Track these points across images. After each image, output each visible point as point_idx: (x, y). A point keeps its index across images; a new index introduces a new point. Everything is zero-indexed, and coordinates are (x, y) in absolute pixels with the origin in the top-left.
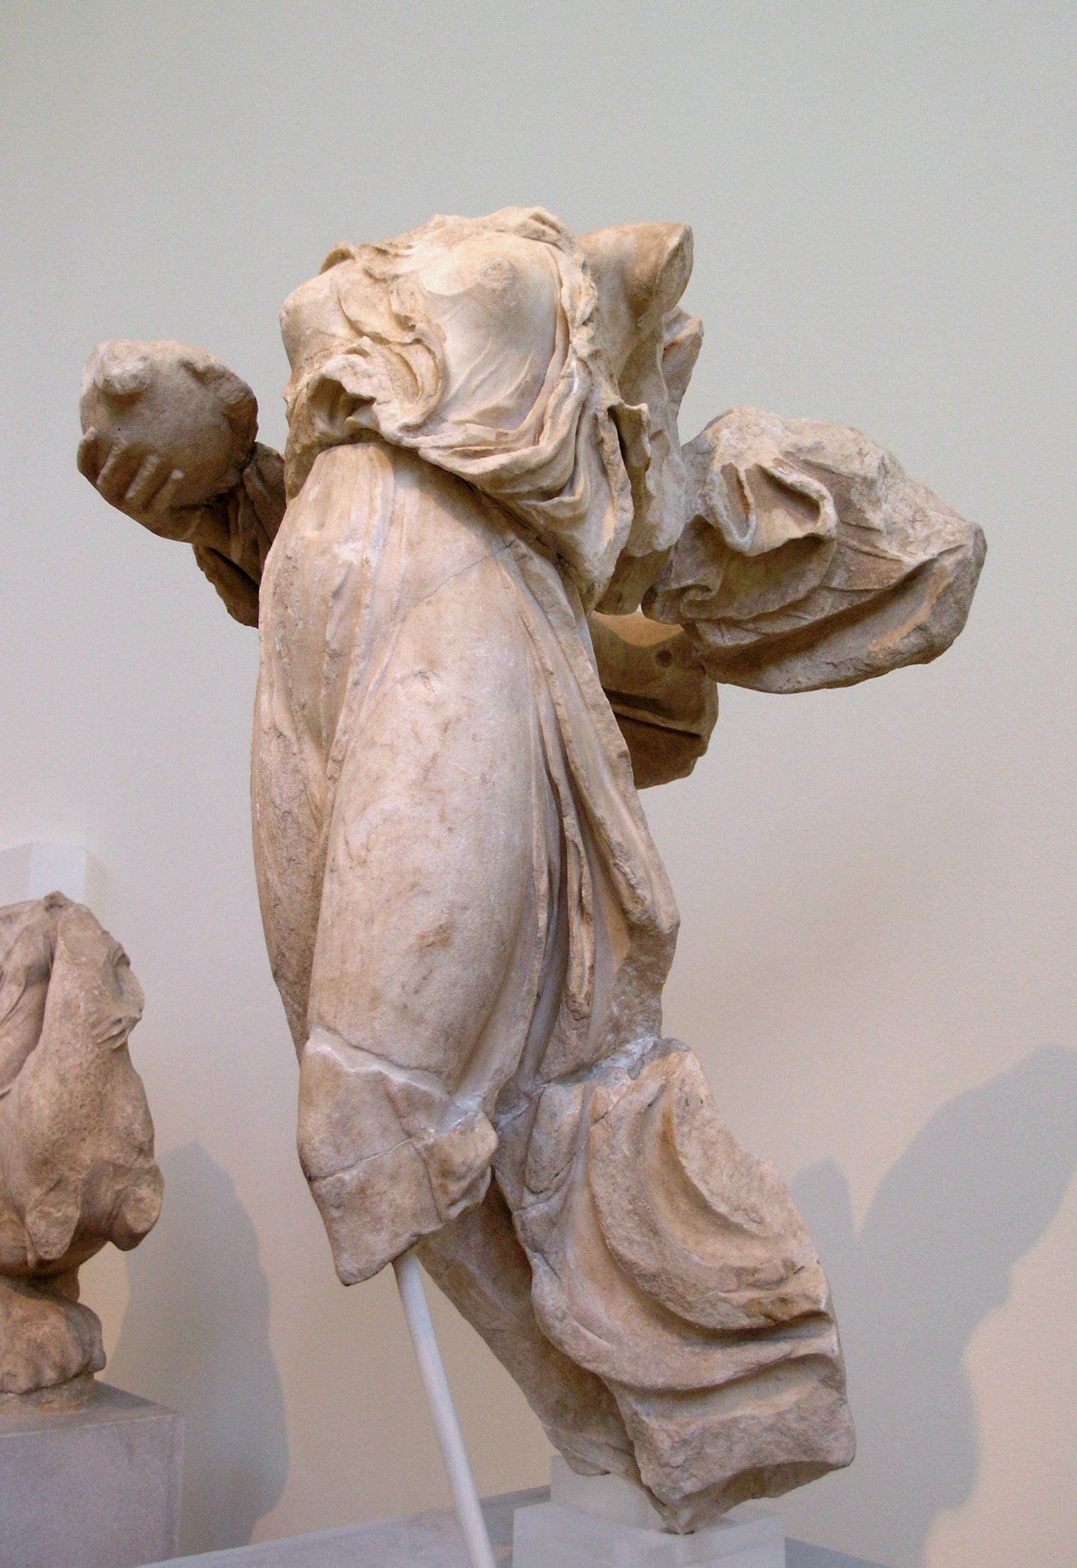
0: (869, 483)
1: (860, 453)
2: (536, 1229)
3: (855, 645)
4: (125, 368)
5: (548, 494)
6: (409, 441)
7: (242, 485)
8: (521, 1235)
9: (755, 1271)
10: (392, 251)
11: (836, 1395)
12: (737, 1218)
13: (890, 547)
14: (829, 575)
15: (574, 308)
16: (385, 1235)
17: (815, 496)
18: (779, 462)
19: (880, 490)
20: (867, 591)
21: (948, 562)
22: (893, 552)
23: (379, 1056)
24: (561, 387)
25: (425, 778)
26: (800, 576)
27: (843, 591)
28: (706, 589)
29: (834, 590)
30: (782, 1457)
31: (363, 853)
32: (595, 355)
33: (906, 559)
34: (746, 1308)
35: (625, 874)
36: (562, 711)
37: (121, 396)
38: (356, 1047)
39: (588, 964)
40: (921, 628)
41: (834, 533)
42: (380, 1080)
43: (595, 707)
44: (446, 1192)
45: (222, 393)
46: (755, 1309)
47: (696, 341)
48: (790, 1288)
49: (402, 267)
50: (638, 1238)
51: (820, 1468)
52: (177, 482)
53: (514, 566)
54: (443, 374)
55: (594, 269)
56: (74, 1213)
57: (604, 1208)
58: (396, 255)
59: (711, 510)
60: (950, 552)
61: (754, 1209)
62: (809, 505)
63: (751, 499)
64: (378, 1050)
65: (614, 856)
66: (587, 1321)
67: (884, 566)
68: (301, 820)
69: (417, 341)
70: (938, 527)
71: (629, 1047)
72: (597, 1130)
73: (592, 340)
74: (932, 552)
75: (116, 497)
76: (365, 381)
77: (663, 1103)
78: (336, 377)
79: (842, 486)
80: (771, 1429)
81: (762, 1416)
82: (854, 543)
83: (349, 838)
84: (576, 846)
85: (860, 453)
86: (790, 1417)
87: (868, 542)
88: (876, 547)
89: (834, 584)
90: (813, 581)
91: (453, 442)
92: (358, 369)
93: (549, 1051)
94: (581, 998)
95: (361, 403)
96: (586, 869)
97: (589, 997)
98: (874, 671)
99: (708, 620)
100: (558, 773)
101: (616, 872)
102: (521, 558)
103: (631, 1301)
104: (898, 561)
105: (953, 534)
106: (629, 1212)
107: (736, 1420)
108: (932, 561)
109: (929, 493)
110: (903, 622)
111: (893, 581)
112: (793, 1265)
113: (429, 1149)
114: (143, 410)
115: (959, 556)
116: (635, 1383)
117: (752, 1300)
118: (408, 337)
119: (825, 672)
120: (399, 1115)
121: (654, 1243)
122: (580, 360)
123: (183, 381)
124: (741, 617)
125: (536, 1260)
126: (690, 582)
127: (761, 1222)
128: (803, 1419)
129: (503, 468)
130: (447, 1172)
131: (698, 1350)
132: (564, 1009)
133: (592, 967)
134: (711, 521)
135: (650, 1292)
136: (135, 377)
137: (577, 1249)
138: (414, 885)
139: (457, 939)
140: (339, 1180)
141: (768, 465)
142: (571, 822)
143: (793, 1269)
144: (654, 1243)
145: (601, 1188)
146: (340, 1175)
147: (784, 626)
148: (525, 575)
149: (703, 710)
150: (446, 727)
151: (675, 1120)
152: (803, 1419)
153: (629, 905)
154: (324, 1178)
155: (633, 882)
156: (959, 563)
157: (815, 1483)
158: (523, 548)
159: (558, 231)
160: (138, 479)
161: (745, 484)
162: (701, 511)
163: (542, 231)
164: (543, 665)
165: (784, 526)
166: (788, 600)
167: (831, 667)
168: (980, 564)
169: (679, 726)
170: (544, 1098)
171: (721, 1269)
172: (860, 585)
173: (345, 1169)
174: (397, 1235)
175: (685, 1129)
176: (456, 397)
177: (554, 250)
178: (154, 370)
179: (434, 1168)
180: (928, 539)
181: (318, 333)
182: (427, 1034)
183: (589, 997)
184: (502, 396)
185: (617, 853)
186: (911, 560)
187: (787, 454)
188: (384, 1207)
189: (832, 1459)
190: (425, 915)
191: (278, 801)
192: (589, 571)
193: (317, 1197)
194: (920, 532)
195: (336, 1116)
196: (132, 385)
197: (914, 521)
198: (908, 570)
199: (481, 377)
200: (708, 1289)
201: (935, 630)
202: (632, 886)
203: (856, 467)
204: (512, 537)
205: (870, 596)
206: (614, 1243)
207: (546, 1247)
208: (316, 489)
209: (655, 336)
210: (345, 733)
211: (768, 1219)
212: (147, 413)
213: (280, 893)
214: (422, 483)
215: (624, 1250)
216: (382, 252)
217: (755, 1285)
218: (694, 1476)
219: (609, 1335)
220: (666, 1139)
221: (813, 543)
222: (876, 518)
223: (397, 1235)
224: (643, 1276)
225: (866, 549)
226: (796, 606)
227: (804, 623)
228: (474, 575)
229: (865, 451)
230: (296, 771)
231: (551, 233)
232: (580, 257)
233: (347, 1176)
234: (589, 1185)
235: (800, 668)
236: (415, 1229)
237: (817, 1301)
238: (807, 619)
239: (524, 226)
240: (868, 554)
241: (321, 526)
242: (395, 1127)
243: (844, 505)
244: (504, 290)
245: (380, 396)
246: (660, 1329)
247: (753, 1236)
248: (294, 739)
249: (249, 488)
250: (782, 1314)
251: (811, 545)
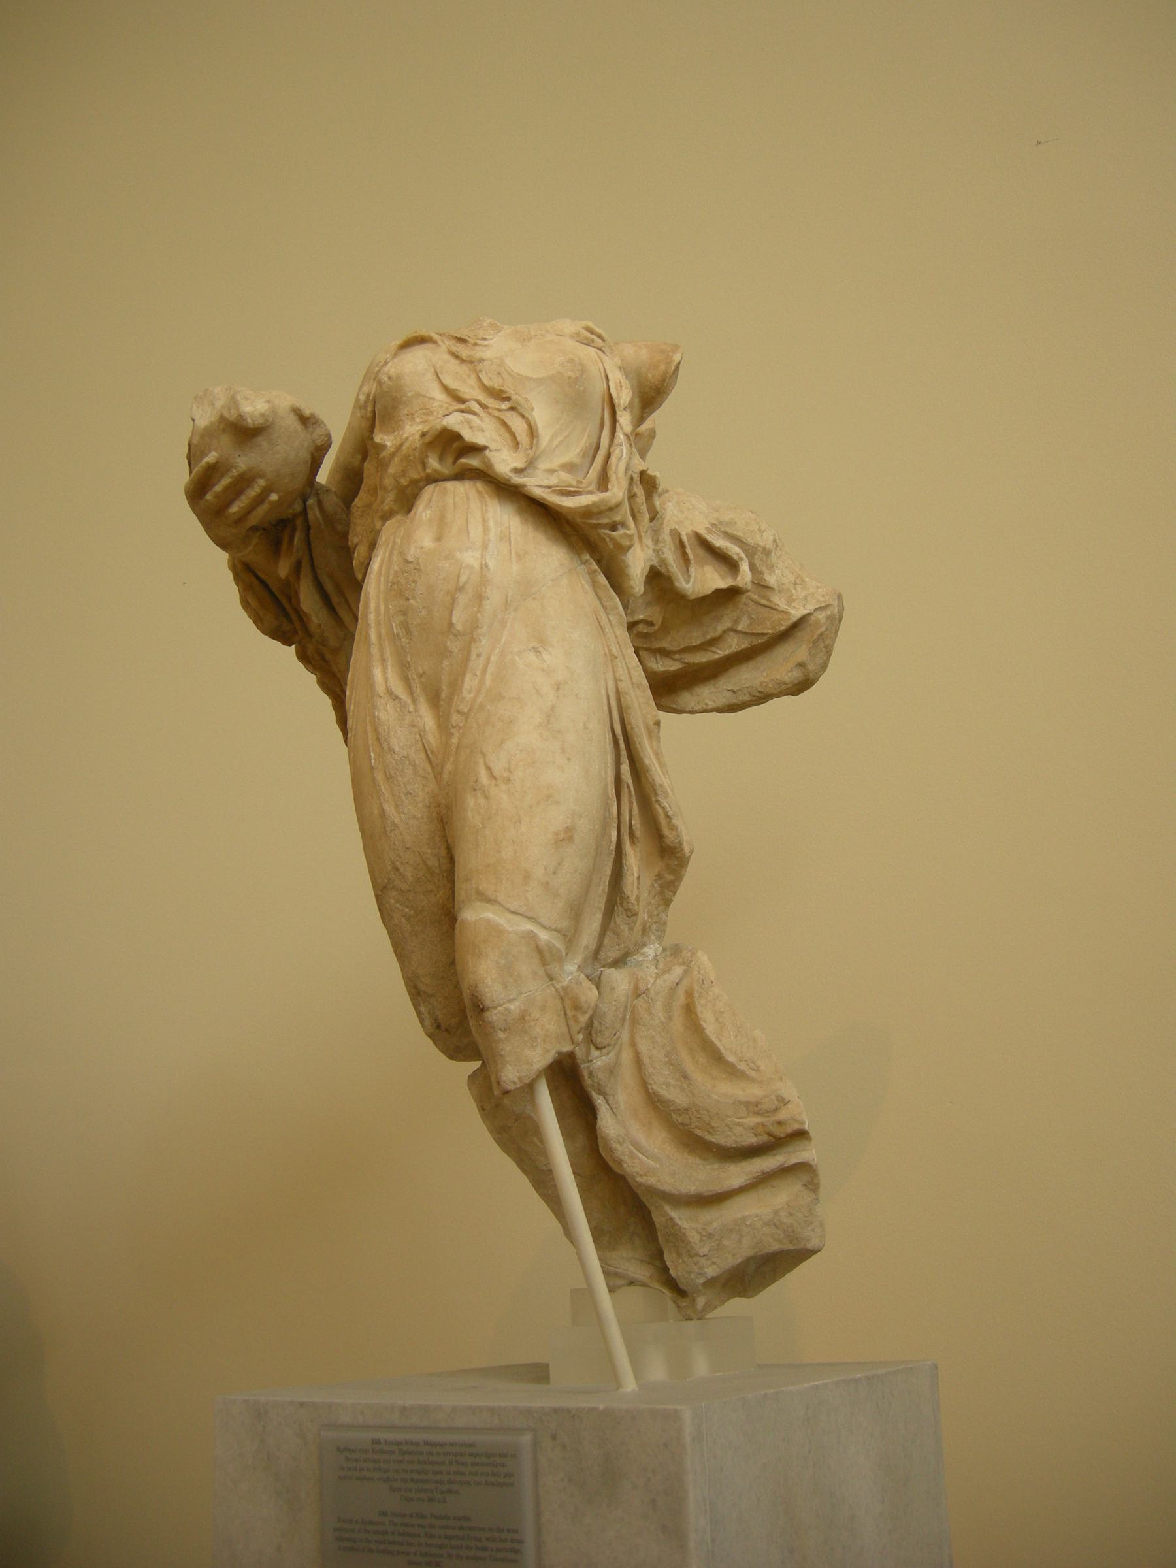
0: (767, 552)
2: (601, 1076)
3: (748, 677)
4: (254, 407)
6: (516, 480)
7: (305, 511)
9: (757, 1104)
10: (472, 341)
11: (813, 1195)
12: (742, 1066)
13: (779, 601)
14: (736, 621)
15: (619, 397)
16: (539, 1050)
17: (736, 558)
19: (773, 559)
20: (763, 634)
22: (783, 605)
23: (530, 918)
25: (549, 722)
26: (718, 619)
27: (746, 633)
28: (651, 624)
29: (741, 632)
30: (776, 1247)
31: (506, 774)
33: (793, 612)
34: (754, 1130)
35: (664, 808)
36: (621, 685)
37: (248, 429)
38: (513, 912)
39: (636, 875)
40: (801, 665)
41: (749, 586)
42: (531, 937)
43: (639, 686)
44: (577, 1021)
45: (315, 436)
46: (760, 1129)
48: (782, 1115)
49: (480, 353)
50: (672, 1082)
51: (804, 1254)
52: (271, 503)
53: (588, 578)
54: (532, 432)
57: (646, 1061)
58: (476, 344)
59: (663, 562)
60: (821, 609)
62: (731, 565)
63: (691, 556)
64: (530, 914)
65: (656, 795)
66: (636, 1145)
67: (776, 616)
68: (417, 762)
69: (512, 409)
70: (812, 590)
71: (646, 950)
72: (640, 1003)
76: (480, 433)
77: (685, 984)
78: (456, 428)
79: (751, 551)
81: (758, 1216)
83: (491, 765)
84: (628, 787)
85: (760, 530)
86: (783, 1213)
87: (765, 597)
88: (770, 601)
89: (739, 628)
90: (727, 623)
91: (551, 484)
92: (473, 424)
93: (606, 941)
94: (633, 899)
95: (475, 449)
96: (635, 805)
97: (638, 898)
98: (762, 698)
99: (647, 649)
100: (618, 731)
101: (657, 806)
102: (592, 573)
104: (787, 613)
105: (823, 596)
106: (666, 1063)
107: (744, 1219)
108: (809, 614)
111: (783, 628)
112: (783, 1099)
113: (565, 989)
114: (262, 441)
116: (674, 1191)
117: (758, 1124)
118: (505, 405)
119: (723, 699)
120: (544, 963)
121: (685, 1086)
122: (626, 435)
123: (292, 422)
124: (672, 649)
125: (599, 1101)
126: (641, 617)
127: (757, 1070)
128: (791, 1214)
129: (594, 504)
130: (577, 1007)
131: (716, 1166)
132: (619, 909)
133: (638, 878)
134: (663, 570)
135: (683, 1124)
136: (263, 415)
138: (549, 797)
140: (506, 1009)
141: (702, 531)
142: (625, 768)
143: (784, 1102)
144: (685, 1086)
145: (643, 1046)
146: (507, 1005)
148: (594, 584)
150: (558, 687)
151: (696, 994)
152: (791, 1214)
153: (666, 831)
154: (495, 1008)
155: (670, 814)
156: (828, 618)
157: (795, 1271)
158: (595, 566)
159: (603, 340)
160: (243, 498)
161: (687, 544)
162: (655, 563)
163: (592, 338)
164: (610, 651)
166: (708, 637)
167: (731, 694)
170: (603, 977)
171: (733, 1103)
173: (510, 1001)
174: (548, 1051)
175: (703, 1001)
177: (600, 353)
178: (274, 412)
179: (568, 1003)
180: (805, 598)
181: (418, 395)
182: (561, 905)
183: (638, 898)
185: (659, 792)
186: (796, 613)
187: (713, 525)
188: (538, 1030)
189: (810, 1246)
190: (557, 818)
191: (397, 749)
192: (632, 588)
194: (800, 593)
195: (503, 962)
196: (260, 421)
197: (795, 584)
198: (794, 619)
199: (560, 439)
200: (727, 1116)
202: (669, 817)
205: (765, 638)
206: (655, 1087)
207: (607, 1090)
208: (428, 512)
210: (470, 692)
211: (763, 1068)
212: (265, 444)
213: (397, 821)
214: (521, 511)
215: (664, 1092)
216: (461, 340)
217: (757, 1113)
218: (714, 1263)
220: (689, 1010)
222: (771, 580)
223: (548, 1051)
225: (764, 602)
226: (713, 642)
227: (717, 656)
228: (565, 581)
229: (763, 528)
230: (413, 726)
234: (633, 1044)
235: (708, 694)
237: (803, 1123)
238: (719, 653)
239: (578, 334)
240: (765, 606)
241: (439, 539)
242: (541, 972)
244: (577, 378)
245: (492, 446)
246: (686, 1155)
248: (409, 701)
249: (310, 516)
250: (780, 1132)
251: (731, 594)
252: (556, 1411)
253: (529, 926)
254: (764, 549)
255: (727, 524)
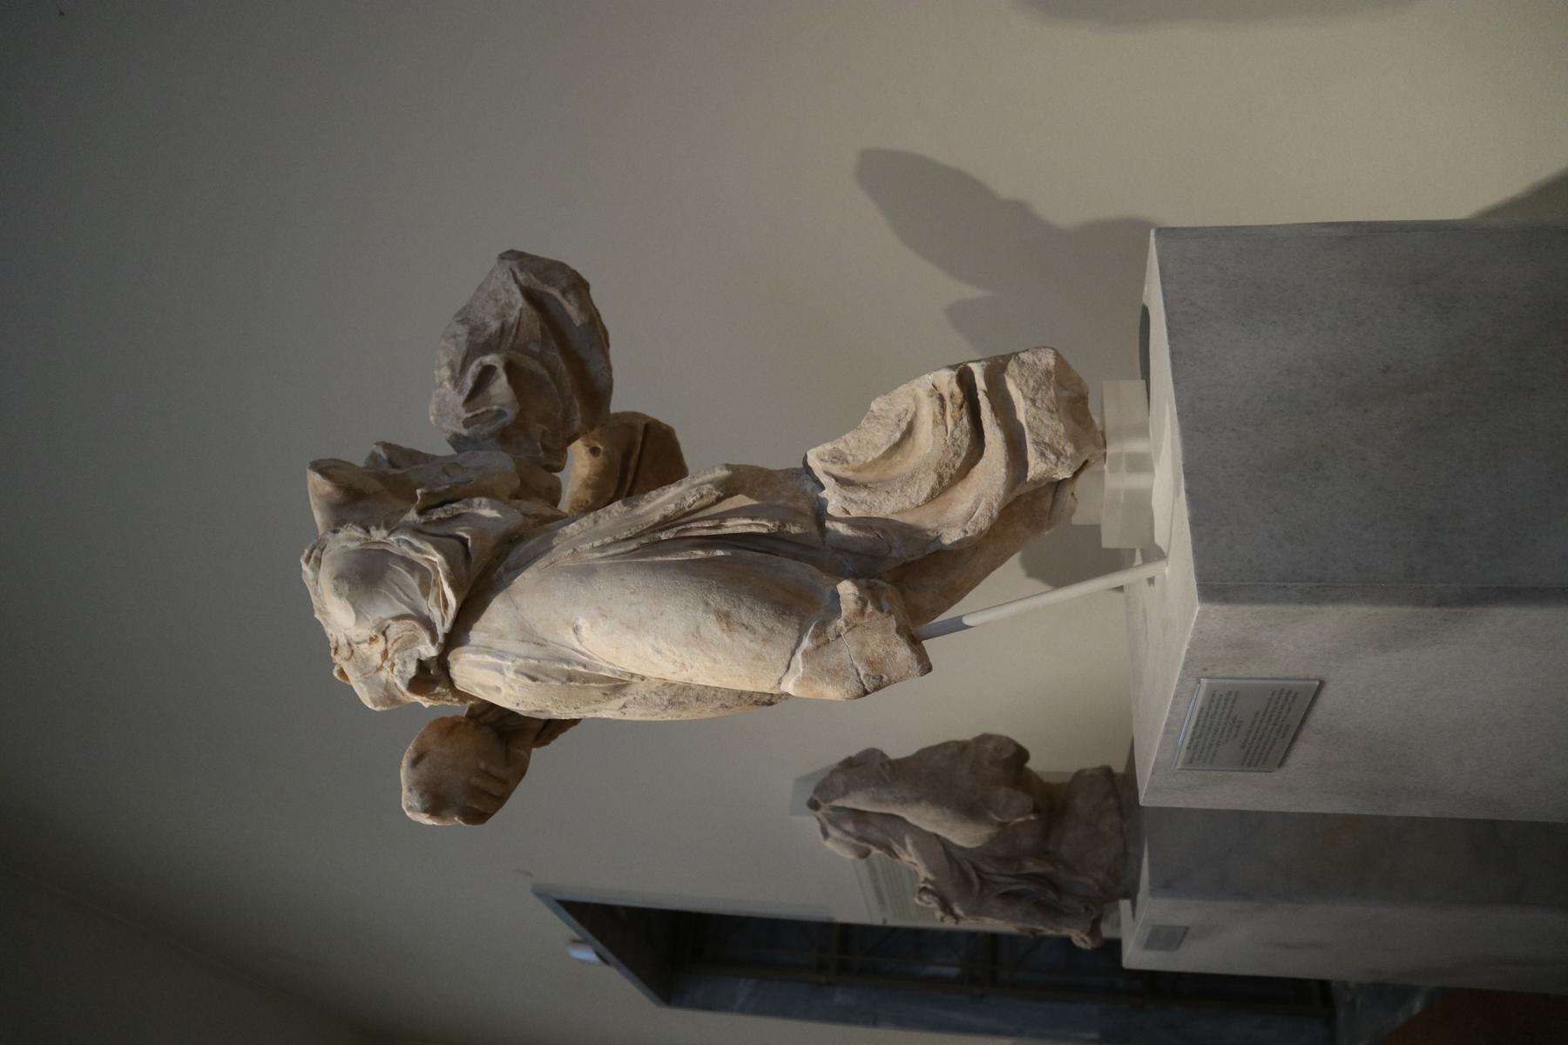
0: (473, 331)
1: (454, 337)
5: (467, 555)
6: (441, 639)
8: (919, 557)
12: (904, 426)
13: (514, 315)
15: (358, 539)
16: (897, 649)
18: (460, 392)
21: (521, 277)
22: (516, 313)
24: (405, 548)
28: (544, 433)
32: (387, 527)
33: (520, 305)
47: (387, 446)
55: (336, 525)
56: (1003, 791)
61: (898, 415)
62: (486, 373)
67: (525, 317)
69: (384, 633)
73: (378, 528)
74: (515, 288)
75: (500, 800)
79: (476, 348)
80: (1033, 401)
82: (511, 340)
102: (508, 570)
103: (959, 487)
109: (480, 288)
110: (561, 305)
115: (517, 271)
137: (926, 520)
139: (725, 608)
141: (462, 399)
147: (568, 381)
149: (630, 422)
156: (521, 270)
158: (501, 569)
165: (500, 387)
168: (522, 255)
169: (640, 439)
172: (538, 333)
176: (415, 610)
179: (858, 621)
180: (507, 291)
184: (413, 582)
186: (519, 301)
187: (456, 385)
193: (877, 689)
201: (564, 283)
203: (463, 339)
204: (495, 576)
209: (382, 478)
215: (926, 491)
219: (977, 503)
221: (510, 367)
222: (495, 325)
224: (940, 483)
231: (316, 552)
232: (329, 536)
233: (862, 673)
236: (893, 631)
243: (487, 348)
245: (416, 656)
247: (915, 415)
252: (1185, 667)
253: (799, 656)
254: (471, 334)
255: (453, 370)
